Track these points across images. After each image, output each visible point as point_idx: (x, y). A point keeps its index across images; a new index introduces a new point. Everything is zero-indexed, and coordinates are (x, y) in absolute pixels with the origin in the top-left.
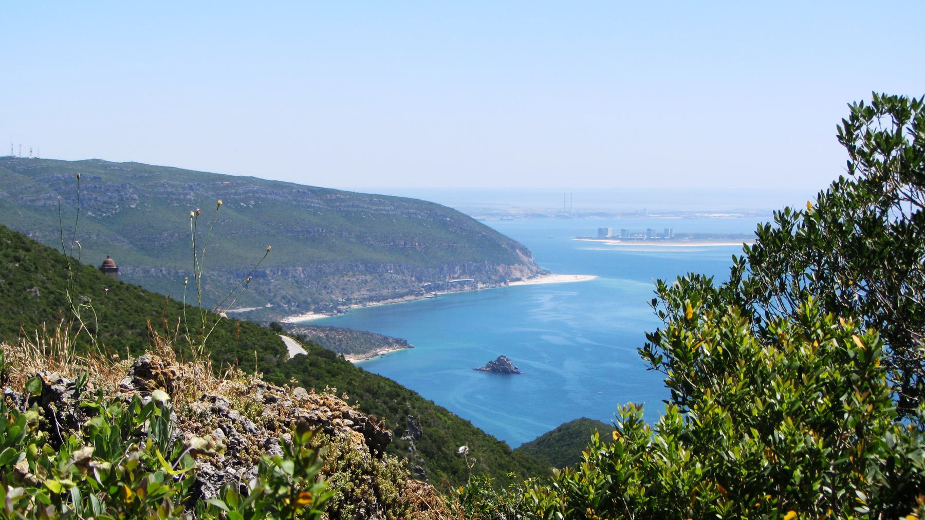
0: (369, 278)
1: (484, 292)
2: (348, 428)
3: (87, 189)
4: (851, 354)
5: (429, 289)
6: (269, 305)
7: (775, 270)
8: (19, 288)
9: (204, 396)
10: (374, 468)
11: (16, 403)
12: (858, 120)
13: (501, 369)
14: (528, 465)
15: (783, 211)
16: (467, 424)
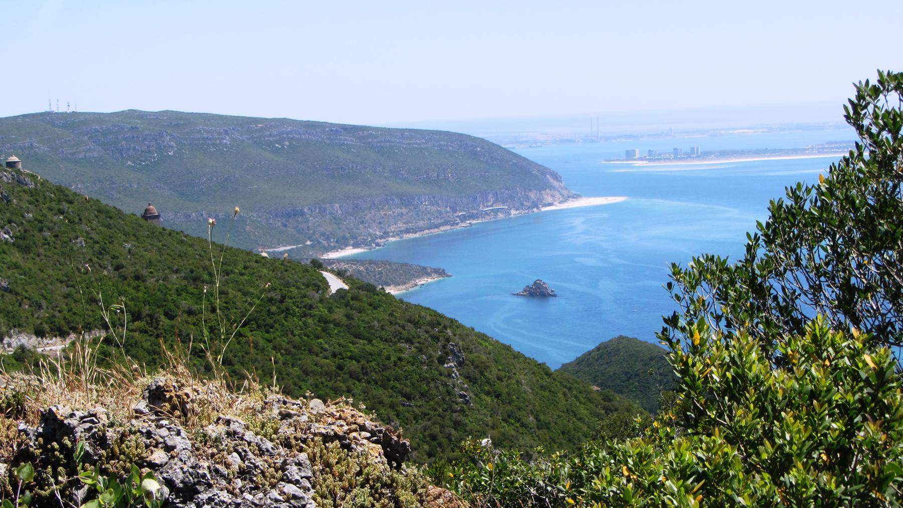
0: (404, 211)
1: (517, 218)
2: (365, 441)
3: (125, 139)
4: (864, 375)
5: (464, 219)
6: (309, 243)
7: (790, 247)
8: (65, 239)
9: (219, 419)
10: (393, 480)
11: (30, 439)
12: (864, 99)
13: (538, 292)
14: (569, 385)
15: (794, 187)
16: (508, 348)
